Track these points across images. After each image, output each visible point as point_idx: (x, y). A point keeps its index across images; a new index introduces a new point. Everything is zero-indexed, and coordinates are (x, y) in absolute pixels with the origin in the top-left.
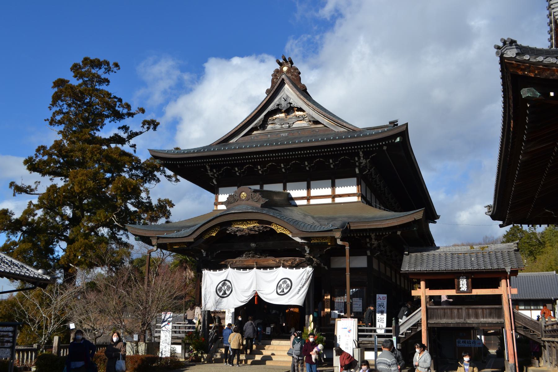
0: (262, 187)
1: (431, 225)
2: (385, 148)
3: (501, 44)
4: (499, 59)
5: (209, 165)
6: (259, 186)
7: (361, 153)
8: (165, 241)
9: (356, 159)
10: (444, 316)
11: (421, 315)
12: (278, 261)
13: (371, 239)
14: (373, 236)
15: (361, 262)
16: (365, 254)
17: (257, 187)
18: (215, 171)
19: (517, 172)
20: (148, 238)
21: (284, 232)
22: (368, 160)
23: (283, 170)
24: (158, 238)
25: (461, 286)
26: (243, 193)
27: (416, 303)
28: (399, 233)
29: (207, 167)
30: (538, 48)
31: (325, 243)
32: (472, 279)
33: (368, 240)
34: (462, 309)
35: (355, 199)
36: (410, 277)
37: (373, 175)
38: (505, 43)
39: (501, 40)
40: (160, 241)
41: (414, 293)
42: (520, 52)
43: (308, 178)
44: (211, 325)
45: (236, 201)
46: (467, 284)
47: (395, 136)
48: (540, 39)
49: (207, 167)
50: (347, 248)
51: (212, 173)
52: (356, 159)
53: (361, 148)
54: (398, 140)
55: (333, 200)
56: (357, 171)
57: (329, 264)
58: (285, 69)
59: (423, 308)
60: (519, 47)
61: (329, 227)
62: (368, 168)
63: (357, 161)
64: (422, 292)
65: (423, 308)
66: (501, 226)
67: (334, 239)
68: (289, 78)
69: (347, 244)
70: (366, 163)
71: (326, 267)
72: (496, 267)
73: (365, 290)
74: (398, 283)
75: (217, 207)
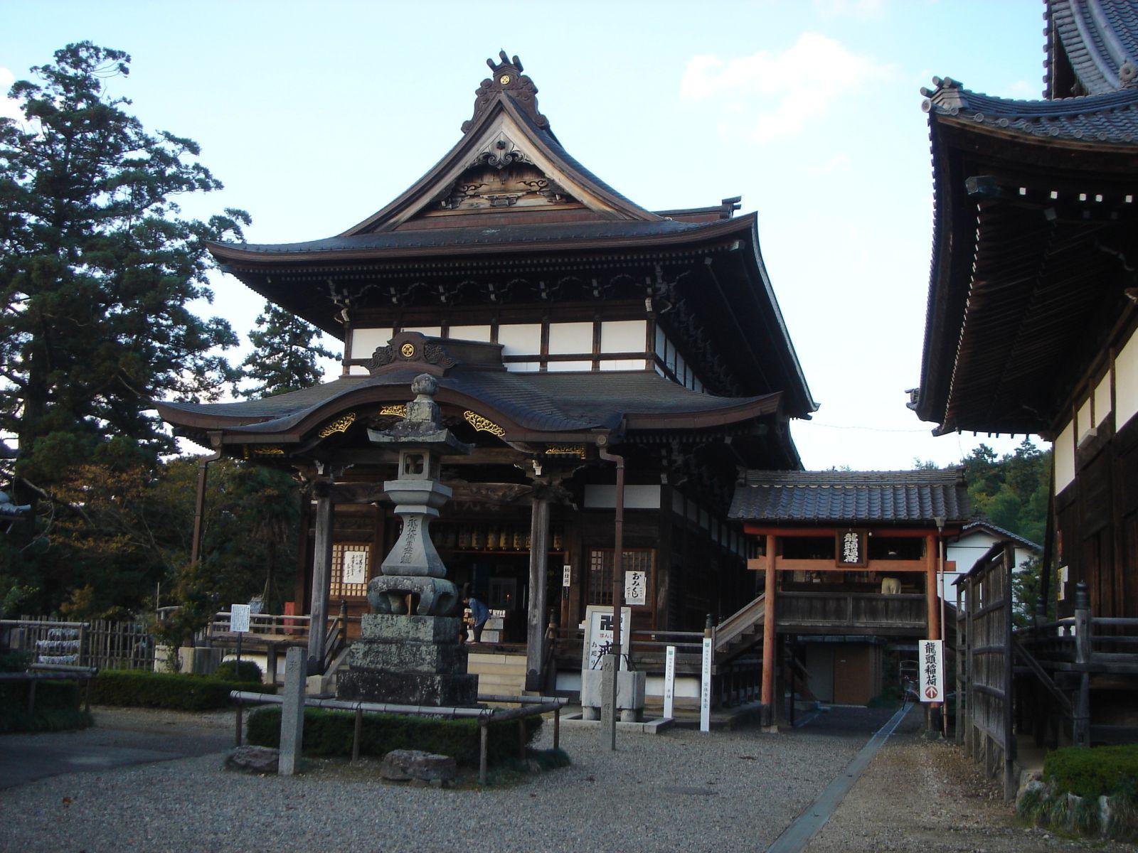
0: (445, 332)
1: (797, 428)
2: (708, 261)
3: (933, 88)
4: (927, 116)
5: (333, 281)
6: (439, 329)
7: (658, 269)
8: (238, 440)
9: (648, 281)
10: (810, 613)
11: (763, 610)
12: (474, 489)
13: (670, 451)
14: (675, 444)
15: (648, 498)
16: (656, 481)
17: (434, 332)
18: (346, 293)
19: (962, 331)
20: (204, 430)
21: (491, 431)
22: (672, 285)
23: (493, 297)
24: (225, 433)
25: (847, 553)
26: (407, 346)
27: (753, 585)
28: (728, 440)
29: (330, 283)
30: (1002, 98)
31: (575, 455)
32: (31, 233)
33: (664, 452)
34: (845, 599)
35: (640, 365)
36: (748, 530)
37: (683, 315)
38: (940, 84)
39: (935, 79)
40: (228, 440)
41: (752, 564)
42: (967, 105)
43: (545, 313)
44: (330, 618)
45: (389, 360)
46: (859, 550)
47: (731, 237)
48: (1018, 77)
49: (330, 283)
50: (620, 466)
51: (339, 298)
52: (648, 281)
53: (658, 260)
54: (736, 246)
55: (596, 366)
56: (648, 303)
57: (579, 499)
58: (505, 80)
59: (768, 594)
60: (967, 96)
61: (583, 424)
62: (673, 300)
63: (649, 286)
64: (765, 564)
65: (768, 594)
66: (936, 433)
67: (592, 449)
68: (512, 100)
69: (619, 460)
70: (668, 290)
71: (574, 505)
72: (916, 515)
73: (653, 555)
74: (724, 543)
75: (424, 393)
